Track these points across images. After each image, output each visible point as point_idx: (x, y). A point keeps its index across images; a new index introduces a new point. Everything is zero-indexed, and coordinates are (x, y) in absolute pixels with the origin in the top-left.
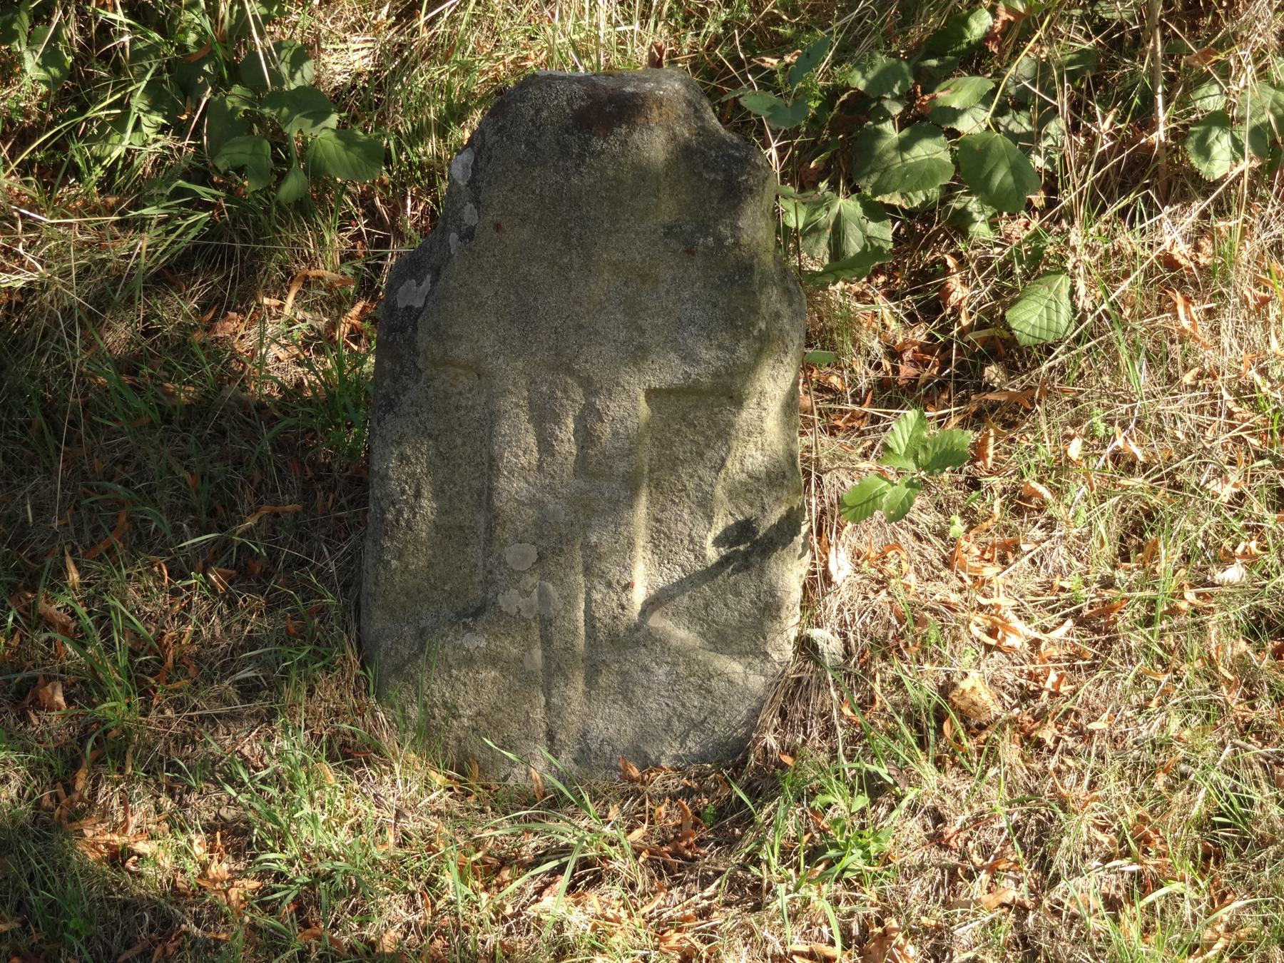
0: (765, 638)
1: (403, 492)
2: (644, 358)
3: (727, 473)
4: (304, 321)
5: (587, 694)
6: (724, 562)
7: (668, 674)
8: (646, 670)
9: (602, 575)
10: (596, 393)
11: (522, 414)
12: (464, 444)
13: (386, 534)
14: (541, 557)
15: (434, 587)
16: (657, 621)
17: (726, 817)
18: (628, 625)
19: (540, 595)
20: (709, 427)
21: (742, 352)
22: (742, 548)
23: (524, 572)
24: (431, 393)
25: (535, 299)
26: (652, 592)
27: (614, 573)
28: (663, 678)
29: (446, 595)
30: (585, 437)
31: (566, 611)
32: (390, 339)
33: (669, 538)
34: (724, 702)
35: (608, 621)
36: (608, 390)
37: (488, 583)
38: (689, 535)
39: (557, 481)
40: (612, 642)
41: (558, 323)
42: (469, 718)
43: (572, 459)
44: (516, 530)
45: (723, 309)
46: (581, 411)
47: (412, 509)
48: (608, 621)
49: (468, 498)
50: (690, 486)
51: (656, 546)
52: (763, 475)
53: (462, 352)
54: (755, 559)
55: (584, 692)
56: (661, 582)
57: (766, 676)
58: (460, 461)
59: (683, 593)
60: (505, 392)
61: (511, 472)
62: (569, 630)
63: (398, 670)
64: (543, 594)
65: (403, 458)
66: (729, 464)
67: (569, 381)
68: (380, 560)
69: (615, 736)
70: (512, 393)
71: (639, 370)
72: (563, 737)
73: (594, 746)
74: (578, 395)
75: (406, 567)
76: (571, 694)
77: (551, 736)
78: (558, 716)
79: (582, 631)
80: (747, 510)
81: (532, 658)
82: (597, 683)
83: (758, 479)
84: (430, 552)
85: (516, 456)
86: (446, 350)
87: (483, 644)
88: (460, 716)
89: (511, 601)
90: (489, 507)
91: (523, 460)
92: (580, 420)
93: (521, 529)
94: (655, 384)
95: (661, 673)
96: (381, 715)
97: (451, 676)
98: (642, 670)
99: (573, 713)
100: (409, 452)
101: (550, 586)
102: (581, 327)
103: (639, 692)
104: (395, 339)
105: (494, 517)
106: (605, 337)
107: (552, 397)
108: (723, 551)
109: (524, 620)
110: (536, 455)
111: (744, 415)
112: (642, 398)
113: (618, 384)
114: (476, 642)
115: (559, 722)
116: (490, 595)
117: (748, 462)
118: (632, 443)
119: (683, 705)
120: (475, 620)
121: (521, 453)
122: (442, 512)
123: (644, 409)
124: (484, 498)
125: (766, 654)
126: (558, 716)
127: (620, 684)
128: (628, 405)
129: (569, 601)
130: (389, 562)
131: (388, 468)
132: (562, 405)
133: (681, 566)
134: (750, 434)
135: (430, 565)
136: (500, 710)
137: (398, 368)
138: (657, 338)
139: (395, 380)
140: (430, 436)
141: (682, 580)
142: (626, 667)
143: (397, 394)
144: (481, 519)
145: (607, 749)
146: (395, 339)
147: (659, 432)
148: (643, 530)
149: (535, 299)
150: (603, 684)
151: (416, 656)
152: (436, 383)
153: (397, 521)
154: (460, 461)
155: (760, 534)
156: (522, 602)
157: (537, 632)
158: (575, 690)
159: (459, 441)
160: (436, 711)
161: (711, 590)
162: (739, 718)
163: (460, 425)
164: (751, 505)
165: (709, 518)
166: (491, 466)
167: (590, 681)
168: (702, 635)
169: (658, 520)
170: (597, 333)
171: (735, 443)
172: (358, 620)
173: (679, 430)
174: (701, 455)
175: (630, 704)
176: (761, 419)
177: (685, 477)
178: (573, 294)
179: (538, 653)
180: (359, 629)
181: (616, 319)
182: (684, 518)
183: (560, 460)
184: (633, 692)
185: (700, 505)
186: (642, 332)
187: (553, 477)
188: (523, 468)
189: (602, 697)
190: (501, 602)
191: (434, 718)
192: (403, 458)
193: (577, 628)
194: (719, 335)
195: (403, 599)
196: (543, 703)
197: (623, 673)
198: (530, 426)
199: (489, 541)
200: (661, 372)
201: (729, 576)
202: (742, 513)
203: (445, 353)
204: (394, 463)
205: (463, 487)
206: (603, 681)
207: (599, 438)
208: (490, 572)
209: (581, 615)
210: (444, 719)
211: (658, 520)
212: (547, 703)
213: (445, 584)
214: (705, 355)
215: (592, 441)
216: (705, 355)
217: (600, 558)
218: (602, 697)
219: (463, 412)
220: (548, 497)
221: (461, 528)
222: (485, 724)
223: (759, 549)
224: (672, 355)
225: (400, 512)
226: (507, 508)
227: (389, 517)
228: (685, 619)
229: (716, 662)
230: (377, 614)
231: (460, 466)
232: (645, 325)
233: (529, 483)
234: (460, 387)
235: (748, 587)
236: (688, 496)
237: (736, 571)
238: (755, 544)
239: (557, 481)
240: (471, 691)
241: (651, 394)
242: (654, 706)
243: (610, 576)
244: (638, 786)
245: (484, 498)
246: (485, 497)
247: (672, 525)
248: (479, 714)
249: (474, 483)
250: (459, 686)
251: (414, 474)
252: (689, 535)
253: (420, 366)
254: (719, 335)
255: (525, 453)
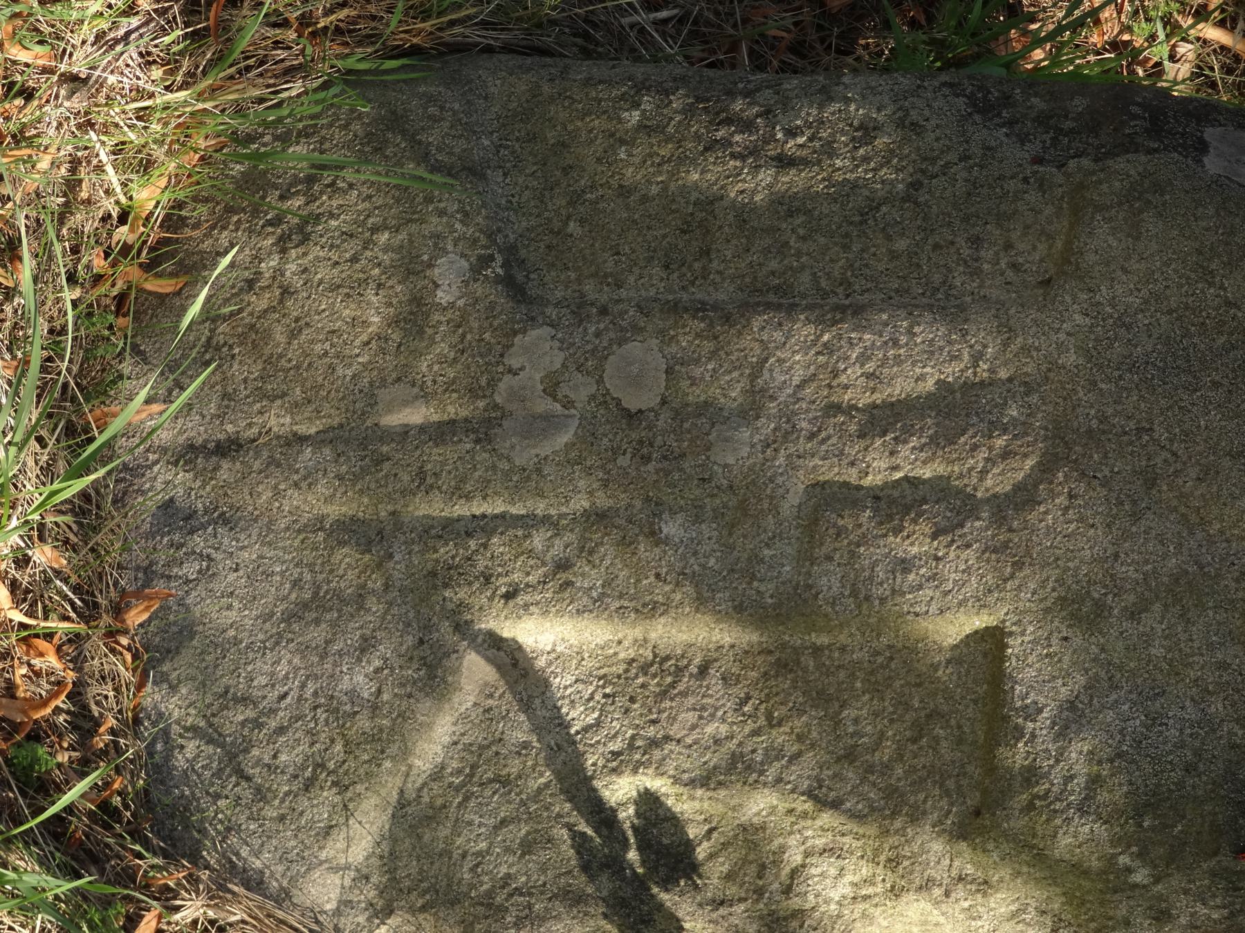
0: (423, 909)
1: (791, 133)
2: (1075, 619)
3: (805, 815)
4: (1172, 58)
5: (318, 524)
6: (603, 816)
7: (353, 694)
8: (366, 646)
9: (587, 551)
10: (999, 519)
11: (956, 367)
12: (894, 255)
13: (699, 99)
14: (632, 417)
15: (575, 198)
16: (475, 670)
17: (24, 794)
18: (469, 607)
19: (547, 417)
20: (913, 769)
21: (1077, 837)
22: (633, 855)
23: (600, 381)
24: (1012, 185)
25: (1216, 385)
26: (541, 663)
27: (589, 577)
28: (345, 684)
29: (556, 225)
30: (898, 503)
31: (507, 475)
32: (1135, 109)
33: (663, 694)
34: (282, 818)
35: (482, 563)
36: (1006, 545)
37: (580, 309)
38: (667, 738)
39: (803, 445)
40: (433, 574)
41: (1161, 434)
42: (279, 272)
43: (852, 476)
44: (697, 361)
45: (1180, 785)
46: (959, 492)
47: (754, 151)
48: (482, 563)
49: (774, 265)
50: (780, 736)
51: (644, 669)
52: (795, 903)
53: (1103, 238)
54: (606, 883)
55: (322, 519)
56: (562, 682)
57: (337, 912)
58: (856, 247)
59: (537, 729)
60: (1007, 330)
61: (828, 349)
62: (463, 480)
63: (395, 121)
64: (549, 423)
65: (867, 132)
66: (827, 818)
67: (1030, 463)
68: (642, 87)
69: (218, 586)
70: (1005, 344)
71: (1047, 611)
72: (223, 474)
73: (198, 542)
74: (999, 481)
75: (622, 142)
76: (320, 489)
77: (228, 448)
78: (272, 462)
79: (461, 509)
80: (721, 866)
81: (406, 403)
82: (342, 543)
83: (787, 890)
84: (654, 190)
85: (863, 358)
86: (1108, 208)
87: (442, 297)
88: (284, 251)
89: (537, 353)
90: (748, 308)
91: (848, 382)
92: (941, 489)
93: (697, 372)
94: (1014, 646)
95: (359, 679)
96: (296, 88)
97: (375, 230)
98: (364, 639)
99: (277, 493)
100: (881, 141)
101: (565, 438)
102: (1151, 483)
103: (317, 635)
104: (1135, 117)
105: (725, 318)
106: (1126, 535)
107: (995, 427)
108: (627, 814)
109: (493, 383)
110: (864, 400)
111: (937, 846)
112: (979, 622)
113: (1018, 566)
114: (449, 282)
115: (257, 465)
116: (552, 312)
117: (828, 866)
118: (883, 600)
119: (281, 730)
120: (498, 280)
121: (870, 367)
122: (743, 215)
123: (955, 627)
124: (772, 297)
125: (388, 911)
126: (272, 462)
127: (337, 594)
128: (968, 591)
129: (525, 480)
130: (636, 105)
131: (848, 101)
132: (975, 447)
133: (598, 724)
134: (893, 863)
135: (624, 191)
136: (293, 335)
137: (1068, 124)
138: (1120, 645)
139: (1043, 120)
140: (915, 185)
141: (565, 725)
142: (373, 605)
143: (1010, 123)
144: (724, 293)
145: (190, 569)
146: (1135, 117)
147: (898, 668)
148: (685, 637)
149: (1216, 385)
150: (338, 556)
151: (424, 157)
152: (1033, 197)
153: (728, 121)
154: (856, 247)
155: (664, 896)
156: (534, 377)
157: (464, 413)
158: (323, 501)
159: (901, 244)
160: (297, 202)
161: (540, 791)
162: (244, 852)
163: (936, 247)
164: (729, 877)
165: (706, 780)
166: (841, 304)
167: (348, 531)
168: (437, 774)
169: (703, 670)
170: (1136, 517)
171: (872, 830)
172: (508, 49)
173: (908, 707)
174: (850, 756)
175: (289, 617)
176: (926, 886)
177: (799, 723)
178: (1226, 462)
179: (416, 415)
180: (489, 50)
181: (1165, 556)
182: (711, 722)
183: (852, 451)
184: (317, 622)
185: (735, 758)
186: (1133, 614)
187: (812, 436)
188: (835, 374)
189: (308, 556)
190: (534, 333)
191: (282, 198)
192: (867, 132)
193: (468, 497)
194: (1123, 778)
195: (552, 136)
196: (302, 429)
197: (360, 599)
198: (930, 385)
199: (675, 308)
200: (1041, 658)
201: (570, 827)
202: (711, 856)
203: (1099, 208)
204: (858, 112)
205: (799, 254)
206: (346, 557)
207: (897, 531)
208: (604, 311)
209: (497, 506)
210: (277, 221)
211: (703, 670)
212: (302, 439)
213: (582, 222)
214: (1078, 750)
215: (890, 517)
216: (1078, 750)
217: (625, 543)
218: (308, 556)
219: (966, 252)
220: (766, 427)
221: (706, 253)
222: (263, 304)
223: (628, 892)
224: (1081, 680)
225: (747, 126)
226: (747, 341)
227: (738, 105)
228: (476, 736)
229: (374, 800)
230: (522, 86)
231: (846, 248)
232: (1151, 620)
233: (800, 387)
234: (1021, 246)
235: (543, 869)
236: (756, 733)
237: (580, 842)
238: (641, 884)
239: (803, 445)
240: (335, 295)
241: (991, 642)
242: (282, 669)
243: (581, 566)
244: (106, 620)
245: (772, 297)
246: (779, 298)
247: (691, 700)
248: (286, 292)
249: (805, 278)
250: (351, 248)
251: (832, 154)
252: (667, 738)
253: (1072, 164)
254: (1123, 778)
255: (869, 376)
